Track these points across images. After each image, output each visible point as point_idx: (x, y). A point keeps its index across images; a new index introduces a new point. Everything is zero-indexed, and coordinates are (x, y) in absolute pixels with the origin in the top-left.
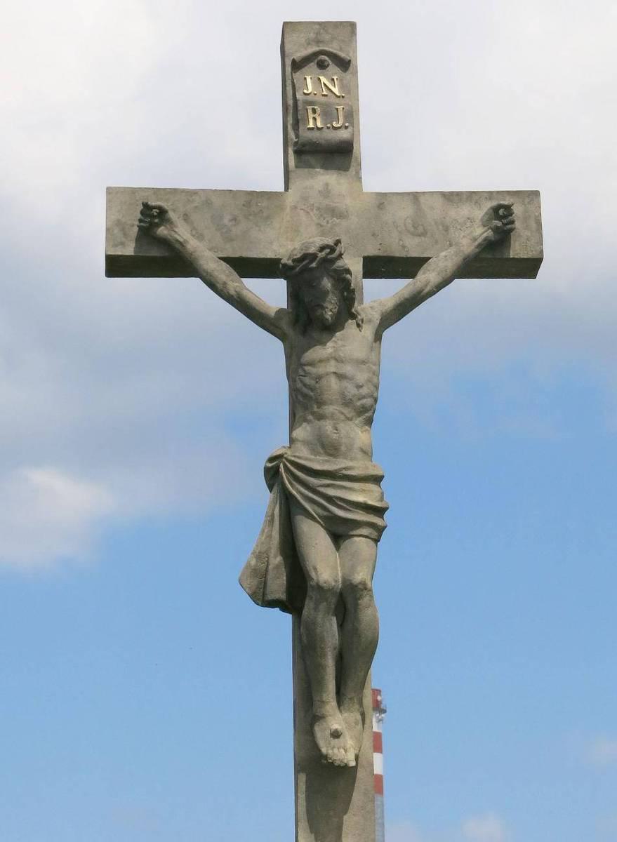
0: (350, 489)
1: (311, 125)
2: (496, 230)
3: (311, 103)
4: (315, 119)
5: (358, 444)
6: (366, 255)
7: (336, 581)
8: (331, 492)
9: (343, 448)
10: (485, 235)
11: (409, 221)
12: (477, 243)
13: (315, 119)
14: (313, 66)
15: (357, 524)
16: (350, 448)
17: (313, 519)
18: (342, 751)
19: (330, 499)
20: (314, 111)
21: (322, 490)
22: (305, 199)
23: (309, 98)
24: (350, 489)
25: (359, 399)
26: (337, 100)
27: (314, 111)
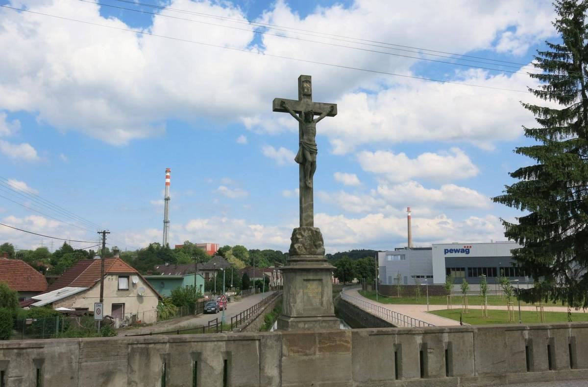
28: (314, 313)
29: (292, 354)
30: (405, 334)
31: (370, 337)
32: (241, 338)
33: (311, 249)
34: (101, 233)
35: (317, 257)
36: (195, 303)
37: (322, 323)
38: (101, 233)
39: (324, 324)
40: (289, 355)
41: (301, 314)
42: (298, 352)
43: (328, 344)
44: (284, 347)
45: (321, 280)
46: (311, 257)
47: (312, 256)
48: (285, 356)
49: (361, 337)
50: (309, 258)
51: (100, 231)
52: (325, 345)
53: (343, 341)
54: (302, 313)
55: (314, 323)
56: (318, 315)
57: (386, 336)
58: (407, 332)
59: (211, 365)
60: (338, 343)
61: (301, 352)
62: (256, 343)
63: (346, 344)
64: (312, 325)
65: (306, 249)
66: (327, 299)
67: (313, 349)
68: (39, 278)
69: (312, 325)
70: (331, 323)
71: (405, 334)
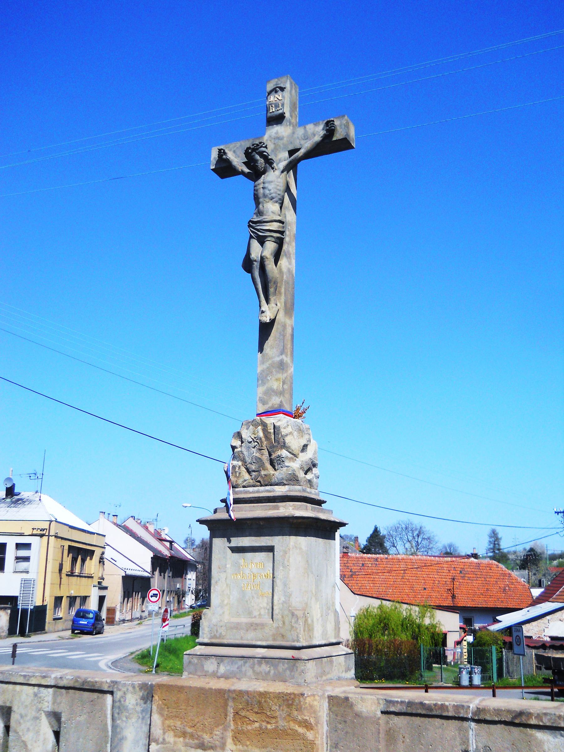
0: (263, 225)
1: (271, 111)
2: (327, 130)
3: (271, 104)
4: (272, 109)
5: (270, 210)
6: (288, 150)
7: (257, 257)
8: (258, 228)
9: (265, 212)
10: (323, 133)
11: (303, 135)
12: (320, 136)
13: (272, 109)
14: (274, 92)
15: (266, 237)
16: (267, 212)
17: (255, 239)
18: (265, 317)
19: (258, 230)
20: (272, 106)
21: (256, 227)
22: (270, 136)
23: (270, 103)
24: (263, 225)
25: (270, 195)
26: (279, 101)
27: (272, 106)
28: (249, 637)
29: (170, 738)
30: (500, 722)
31: (385, 717)
32: (77, 685)
33: (259, 471)
34: (560, 512)
35: (274, 491)
36: (390, 608)
37: (260, 664)
38: (560, 512)
39: (265, 668)
40: (164, 739)
41: (221, 636)
42: (184, 734)
43: (257, 725)
44: (156, 717)
45: (270, 549)
46: (258, 492)
47: (262, 488)
48: (157, 742)
49: (358, 715)
50: (253, 492)
51: (559, 511)
52: (249, 728)
53: (295, 720)
54: (223, 633)
55: (240, 662)
56: (259, 643)
57: (438, 721)
58: (508, 718)
59: (23, 739)
60: (282, 723)
61: (192, 736)
62: (105, 700)
63: (301, 730)
64: (234, 668)
65: (249, 472)
66: (283, 599)
67: (218, 732)
68: (556, 579)
69: (234, 668)
70: (282, 666)
71: (500, 722)
